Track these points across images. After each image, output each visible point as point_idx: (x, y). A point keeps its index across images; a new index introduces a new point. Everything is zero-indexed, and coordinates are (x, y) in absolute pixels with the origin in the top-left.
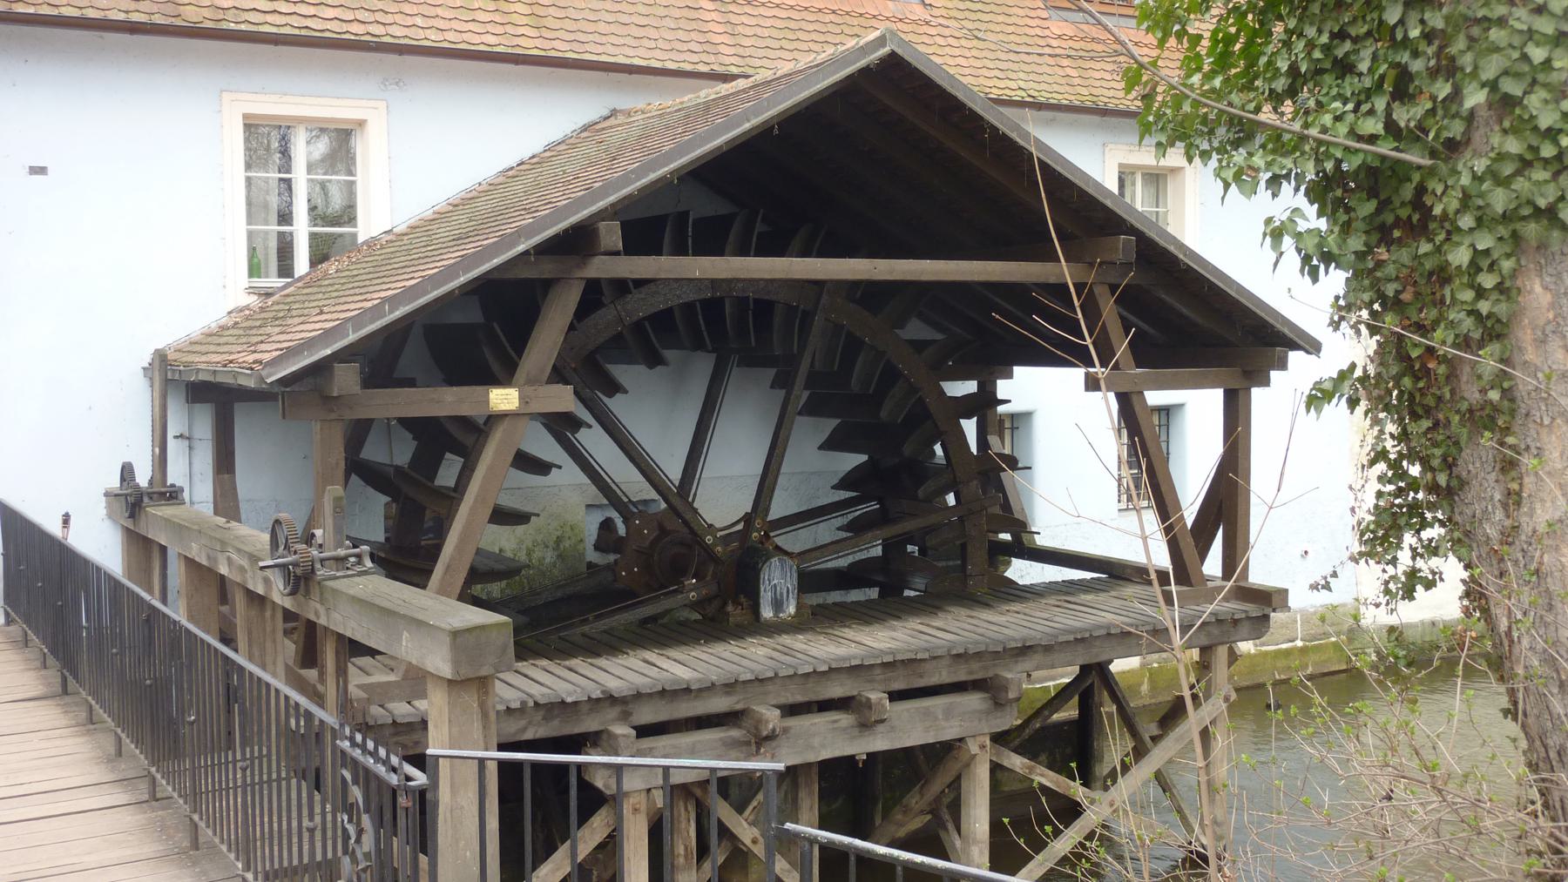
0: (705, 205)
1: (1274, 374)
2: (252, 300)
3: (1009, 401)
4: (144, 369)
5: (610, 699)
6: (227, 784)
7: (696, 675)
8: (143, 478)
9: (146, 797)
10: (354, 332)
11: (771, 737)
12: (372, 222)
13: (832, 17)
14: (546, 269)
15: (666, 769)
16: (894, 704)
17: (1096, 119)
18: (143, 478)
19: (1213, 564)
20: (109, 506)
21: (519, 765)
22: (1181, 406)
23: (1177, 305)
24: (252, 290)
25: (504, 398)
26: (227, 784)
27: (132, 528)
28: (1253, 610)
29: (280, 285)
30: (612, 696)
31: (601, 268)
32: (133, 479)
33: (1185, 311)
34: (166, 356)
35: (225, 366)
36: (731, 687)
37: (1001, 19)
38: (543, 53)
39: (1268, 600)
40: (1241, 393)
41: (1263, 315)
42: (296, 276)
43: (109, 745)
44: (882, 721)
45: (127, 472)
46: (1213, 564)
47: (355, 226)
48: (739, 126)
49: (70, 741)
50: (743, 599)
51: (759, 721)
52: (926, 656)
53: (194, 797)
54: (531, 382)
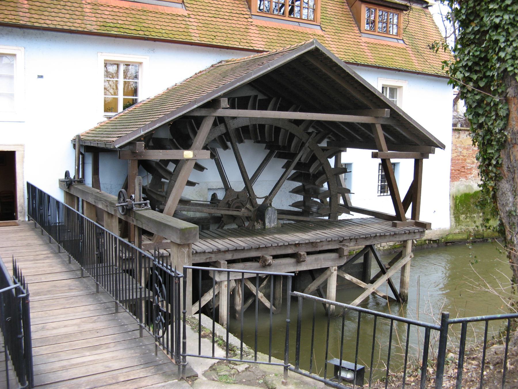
0: (250, 93)
1: (430, 155)
4: (72, 141)
5: (219, 251)
6: (105, 273)
7: (246, 245)
8: (72, 176)
9: (80, 276)
10: (143, 131)
11: (269, 265)
12: (142, 96)
13: (293, 33)
15: (243, 273)
16: (308, 256)
17: (376, 69)
19: (408, 214)
20: (60, 184)
21: (198, 270)
22: (398, 163)
23: (401, 132)
25: (188, 154)
26: (105, 273)
27: (68, 191)
28: (421, 230)
29: (114, 115)
30: (220, 251)
31: (220, 112)
32: (69, 176)
33: (404, 133)
34: (80, 137)
36: (258, 249)
37: (346, 36)
38: (200, 42)
39: (425, 226)
40: (420, 161)
41: (428, 136)
42: (119, 112)
43: (67, 259)
44: (304, 261)
45: (67, 174)
46: (408, 214)
48: (266, 68)
50: (260, 221)
51: (265, 260)
52: (319, 241)
53: (97, 277)
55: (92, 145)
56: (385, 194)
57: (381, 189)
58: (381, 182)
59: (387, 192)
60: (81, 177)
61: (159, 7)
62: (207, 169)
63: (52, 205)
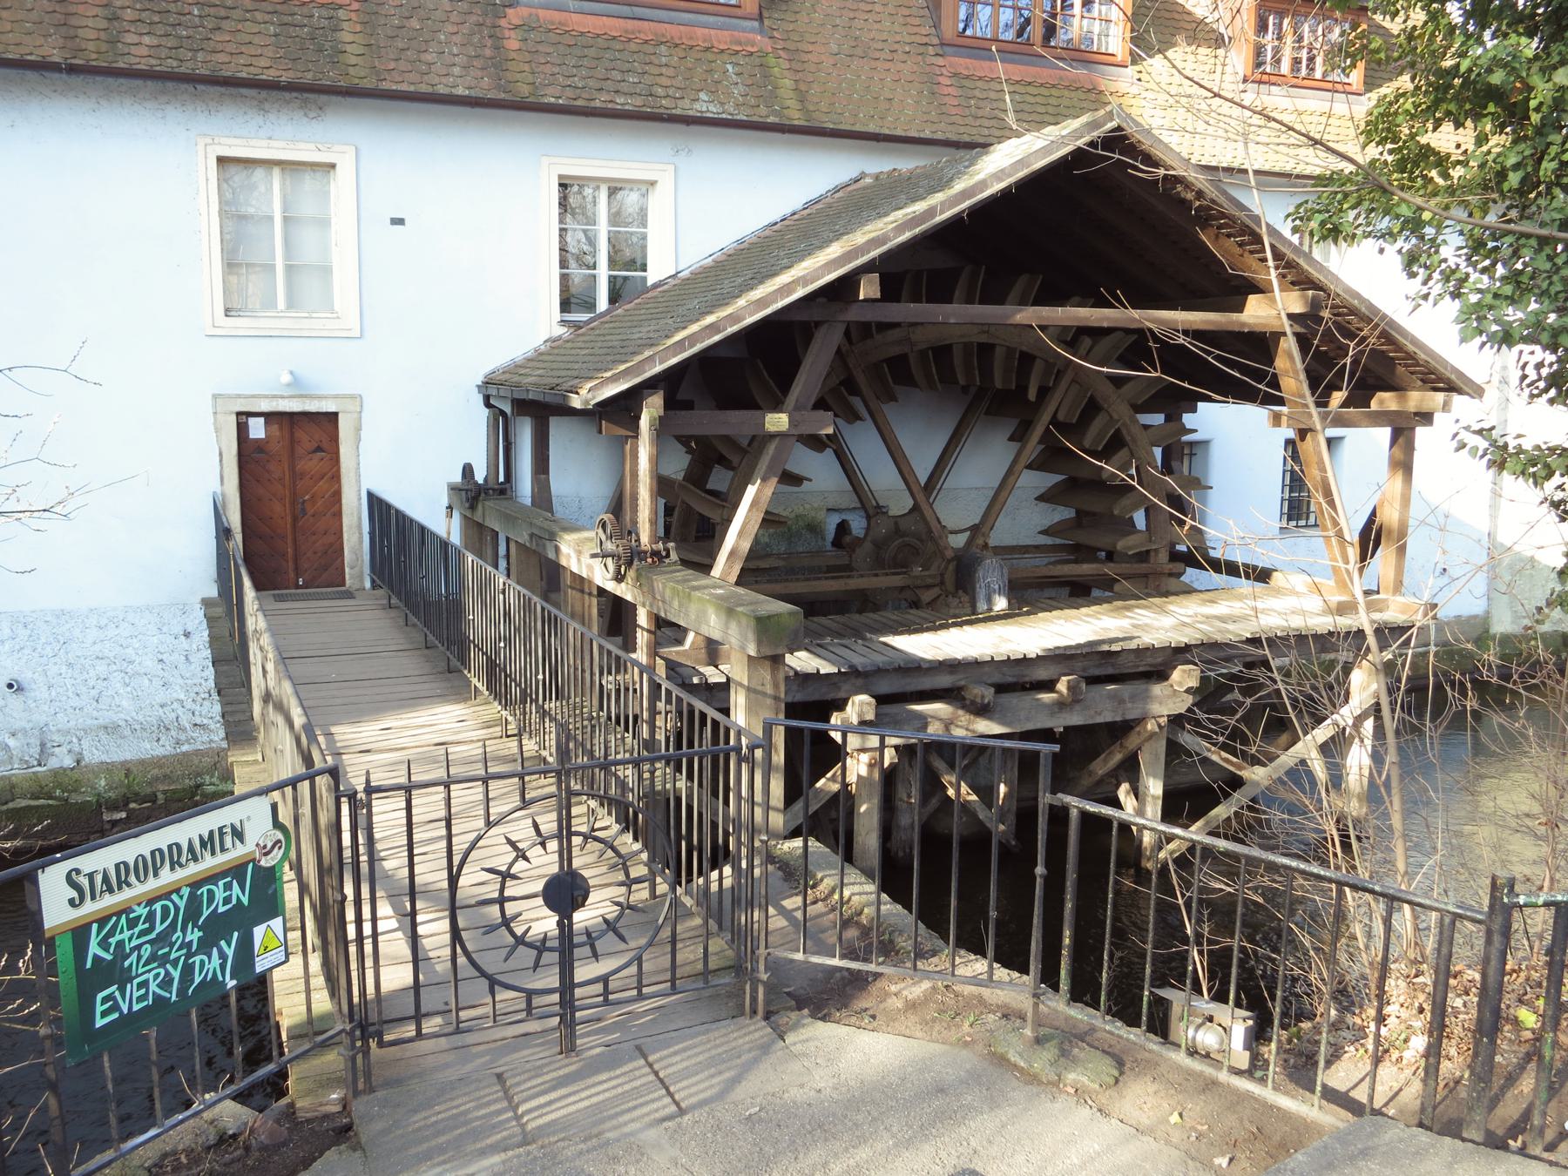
2: (560, 331)
3: (1196, 431)
4: (478, 386)
8: (480, 477)
14: (814, 315)
18: (480, 477)
21: (800, 730)
24: (563, 322)
25: (777, 421)
27: (469, 515)
35: (552, 389)
45: (468, 471)
47: (645, 270)
49: (434, 685)
54: (797, 408)
55: (530, 397)
56: (1302, 523)
57: (1299, 508)
58: (1291, 492)
59: (1307, 519)
60: (501, 479)
61: (700, 32)
62: (810, 480)
63: (432, 550)
